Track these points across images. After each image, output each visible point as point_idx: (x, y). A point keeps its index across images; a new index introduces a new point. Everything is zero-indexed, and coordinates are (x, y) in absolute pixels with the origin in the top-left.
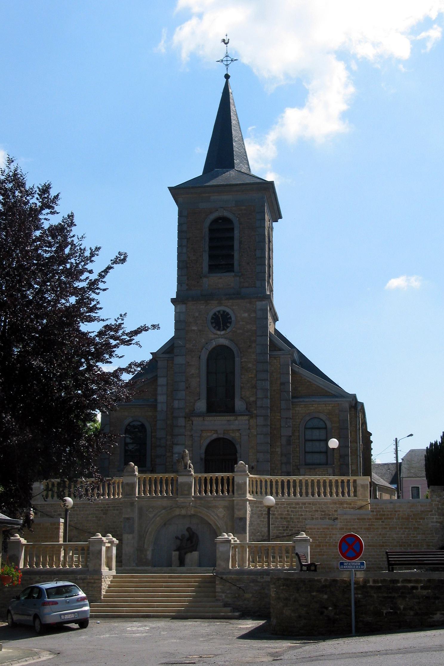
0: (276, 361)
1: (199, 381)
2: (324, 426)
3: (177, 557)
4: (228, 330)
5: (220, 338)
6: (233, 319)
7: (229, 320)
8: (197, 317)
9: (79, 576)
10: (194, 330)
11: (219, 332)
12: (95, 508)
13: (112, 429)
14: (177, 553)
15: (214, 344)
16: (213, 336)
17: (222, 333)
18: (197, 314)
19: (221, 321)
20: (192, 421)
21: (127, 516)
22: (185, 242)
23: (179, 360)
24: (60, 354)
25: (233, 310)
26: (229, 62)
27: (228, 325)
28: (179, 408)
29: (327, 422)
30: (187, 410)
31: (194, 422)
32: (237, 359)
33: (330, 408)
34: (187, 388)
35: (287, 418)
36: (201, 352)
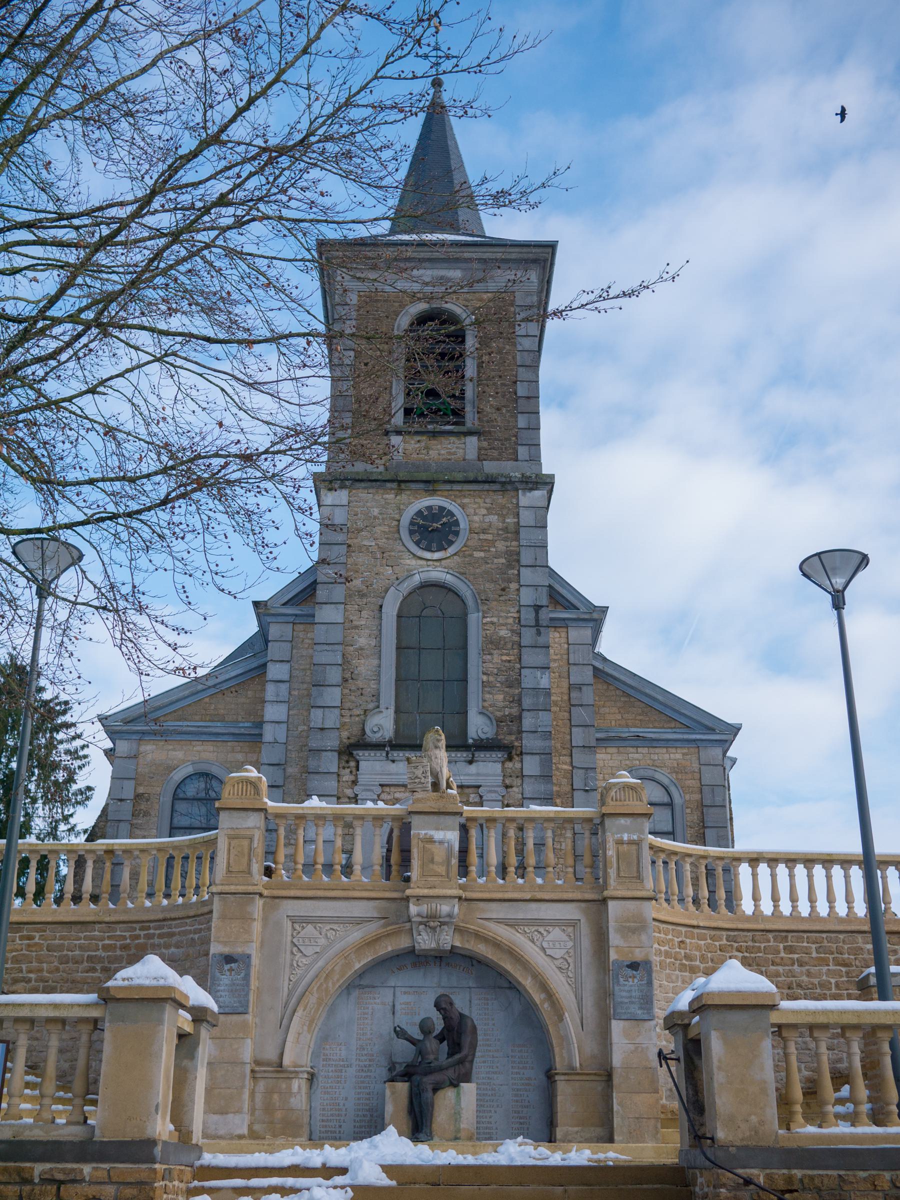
0: (557, 635)
1: (379, 665)
2: (666, 799)
3: (404, 1101)
4: (451, 550)
5: (434, 566)
6: (462, 525)
7: (453, 528)
8: (375, 518)
9: (39, 1168)
10: (368, 547)
11: (428, 555)
12: (102, 939)
13: (141, 790)
14: (402, 1087)
15: (417, 579)
16: (413, 562)
17: (437, 555)
18: (376, 512)
19: (434, 531)
20: (358, 762)
21: (226, 950)
22: (522, 390)
23: (327, 614)
24: (25, 462)
25: (463, 506)
26: (434, 53)
27: (417, 537)
28: (322, 729)
29: (673, 789)
30: (345, 734)
31: (362, 764)
32: (473, 618)
33: (679, 756)
34: (345, 680)
35: (587, 769)
36: (383, 598)
